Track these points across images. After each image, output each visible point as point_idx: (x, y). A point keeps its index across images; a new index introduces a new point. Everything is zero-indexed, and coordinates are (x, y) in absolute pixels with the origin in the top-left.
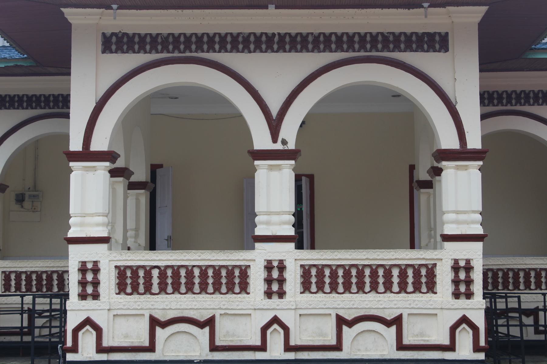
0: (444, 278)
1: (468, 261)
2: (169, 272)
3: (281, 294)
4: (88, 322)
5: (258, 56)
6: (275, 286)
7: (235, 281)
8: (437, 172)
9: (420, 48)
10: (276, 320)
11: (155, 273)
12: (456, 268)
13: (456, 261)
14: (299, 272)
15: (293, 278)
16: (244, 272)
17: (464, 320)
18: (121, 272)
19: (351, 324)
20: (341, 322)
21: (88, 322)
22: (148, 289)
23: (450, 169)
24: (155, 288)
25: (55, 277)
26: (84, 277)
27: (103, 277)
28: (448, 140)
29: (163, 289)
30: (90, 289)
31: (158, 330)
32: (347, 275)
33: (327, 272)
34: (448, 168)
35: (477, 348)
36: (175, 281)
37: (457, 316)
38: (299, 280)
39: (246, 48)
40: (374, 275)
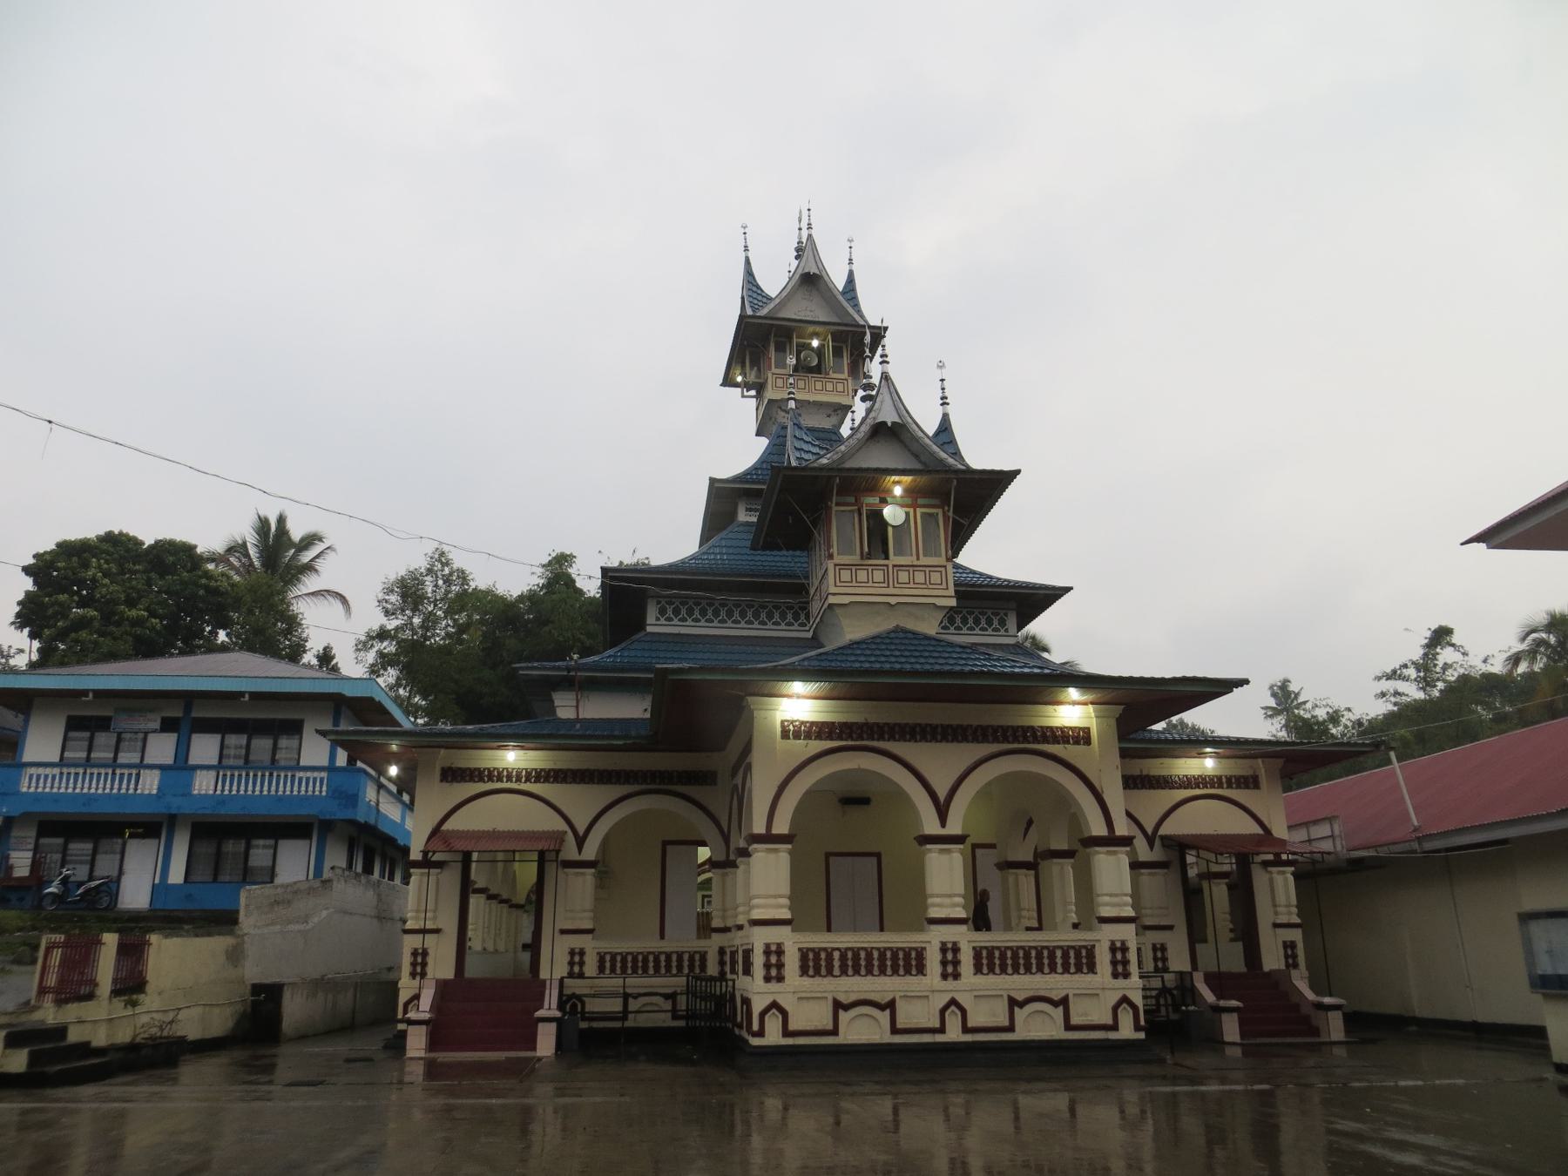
0: (1103, 958)
1: (1123, 943)
2: (850, 955)
3: (780, 979)
4: (775, 1005)
5: (923, 746)
6: (950, 968)
7: (912, 962)
8: (745, 853)
9: (903, 738)
10: (953, 1002)
11: (836, 955)
12: (944, 950)
13: (1113, 943)
14: (971, 953)
15: (967, 958)
16: (920, 954)
17: (1125, 999)
18: (804, 954)
19: (847, 1007)
20: (1013, 1003)
21: (775, 1005)
22: (830, 972)
23: (760, 854)
24: (836, 971)
25: (651, 958)
26: (1124, 956)
27: (587, 959)
28: (1098, 829)
29: (844, 972)
30: (775, 972)
31: (841, 1012)
32: (1015, 957)
33: (997, 954)
34: (756, 850)
35: (1137, 1028)
36: (855, 963)
37: (946, 999)
38: (972, 962)
39: (913, 738)
40: (1039, 957)
